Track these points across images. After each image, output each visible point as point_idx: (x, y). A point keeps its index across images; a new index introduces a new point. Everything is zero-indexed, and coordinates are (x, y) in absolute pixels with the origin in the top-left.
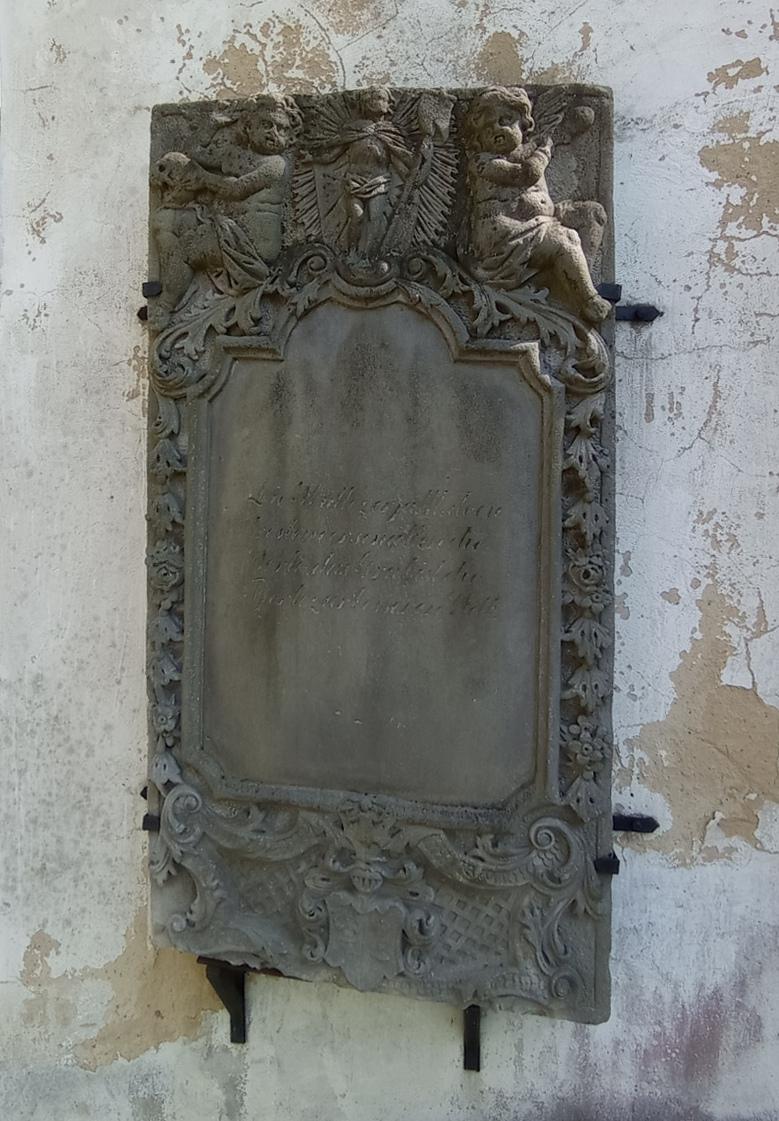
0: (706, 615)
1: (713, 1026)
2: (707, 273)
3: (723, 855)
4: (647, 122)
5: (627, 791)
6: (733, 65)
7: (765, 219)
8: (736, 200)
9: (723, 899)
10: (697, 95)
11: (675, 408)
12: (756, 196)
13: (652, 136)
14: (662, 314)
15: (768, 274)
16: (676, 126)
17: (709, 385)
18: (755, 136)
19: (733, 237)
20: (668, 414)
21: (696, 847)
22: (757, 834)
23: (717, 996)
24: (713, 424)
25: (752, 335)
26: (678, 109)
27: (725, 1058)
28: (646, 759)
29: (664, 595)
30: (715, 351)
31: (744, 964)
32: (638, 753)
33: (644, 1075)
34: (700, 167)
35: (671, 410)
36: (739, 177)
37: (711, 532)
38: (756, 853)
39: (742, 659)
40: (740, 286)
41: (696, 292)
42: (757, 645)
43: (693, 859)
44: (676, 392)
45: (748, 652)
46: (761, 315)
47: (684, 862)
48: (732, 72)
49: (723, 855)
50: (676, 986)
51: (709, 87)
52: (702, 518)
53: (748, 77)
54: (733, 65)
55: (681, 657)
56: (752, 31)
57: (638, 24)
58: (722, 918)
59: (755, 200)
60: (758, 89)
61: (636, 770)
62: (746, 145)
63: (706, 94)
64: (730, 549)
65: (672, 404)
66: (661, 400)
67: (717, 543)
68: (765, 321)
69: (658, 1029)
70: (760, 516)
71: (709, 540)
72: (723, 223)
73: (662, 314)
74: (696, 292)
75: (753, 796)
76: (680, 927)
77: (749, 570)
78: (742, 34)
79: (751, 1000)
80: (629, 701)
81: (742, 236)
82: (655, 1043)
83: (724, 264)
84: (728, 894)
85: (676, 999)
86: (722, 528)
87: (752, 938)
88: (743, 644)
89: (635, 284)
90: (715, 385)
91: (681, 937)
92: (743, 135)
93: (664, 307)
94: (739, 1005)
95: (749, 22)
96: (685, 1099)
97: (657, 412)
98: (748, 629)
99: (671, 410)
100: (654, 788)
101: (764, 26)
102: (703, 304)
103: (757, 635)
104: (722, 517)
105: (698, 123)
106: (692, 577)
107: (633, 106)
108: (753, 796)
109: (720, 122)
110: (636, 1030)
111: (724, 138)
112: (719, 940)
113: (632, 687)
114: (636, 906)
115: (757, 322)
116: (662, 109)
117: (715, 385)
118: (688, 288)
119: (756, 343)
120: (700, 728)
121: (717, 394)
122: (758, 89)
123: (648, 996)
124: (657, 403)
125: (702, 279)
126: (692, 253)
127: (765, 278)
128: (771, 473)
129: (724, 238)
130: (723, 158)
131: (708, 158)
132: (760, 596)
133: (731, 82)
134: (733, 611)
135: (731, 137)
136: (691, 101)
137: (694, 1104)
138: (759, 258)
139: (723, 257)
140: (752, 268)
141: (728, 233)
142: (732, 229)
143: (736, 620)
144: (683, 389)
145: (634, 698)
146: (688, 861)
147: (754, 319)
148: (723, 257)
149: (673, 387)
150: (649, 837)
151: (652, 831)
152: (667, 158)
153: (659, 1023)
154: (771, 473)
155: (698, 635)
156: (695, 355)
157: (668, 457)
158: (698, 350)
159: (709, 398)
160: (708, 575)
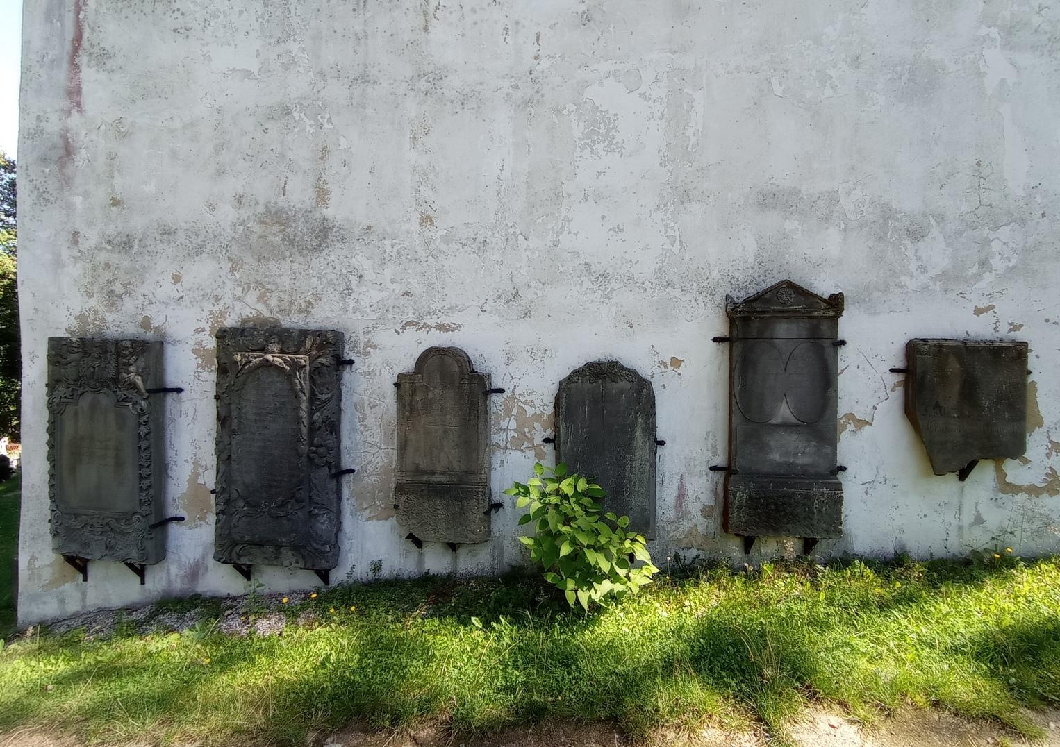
11: (186, 414)
13: (181, 345)
32: (180, 501)
51: (194, 333)
52: (193, 442)
66: (183, 412)
67: (196, 448)
97: (182, 415)
100: (184, 510)
105: (191, 343)
111: (197, 347)
131: (194, 351)
141: (199, 370)
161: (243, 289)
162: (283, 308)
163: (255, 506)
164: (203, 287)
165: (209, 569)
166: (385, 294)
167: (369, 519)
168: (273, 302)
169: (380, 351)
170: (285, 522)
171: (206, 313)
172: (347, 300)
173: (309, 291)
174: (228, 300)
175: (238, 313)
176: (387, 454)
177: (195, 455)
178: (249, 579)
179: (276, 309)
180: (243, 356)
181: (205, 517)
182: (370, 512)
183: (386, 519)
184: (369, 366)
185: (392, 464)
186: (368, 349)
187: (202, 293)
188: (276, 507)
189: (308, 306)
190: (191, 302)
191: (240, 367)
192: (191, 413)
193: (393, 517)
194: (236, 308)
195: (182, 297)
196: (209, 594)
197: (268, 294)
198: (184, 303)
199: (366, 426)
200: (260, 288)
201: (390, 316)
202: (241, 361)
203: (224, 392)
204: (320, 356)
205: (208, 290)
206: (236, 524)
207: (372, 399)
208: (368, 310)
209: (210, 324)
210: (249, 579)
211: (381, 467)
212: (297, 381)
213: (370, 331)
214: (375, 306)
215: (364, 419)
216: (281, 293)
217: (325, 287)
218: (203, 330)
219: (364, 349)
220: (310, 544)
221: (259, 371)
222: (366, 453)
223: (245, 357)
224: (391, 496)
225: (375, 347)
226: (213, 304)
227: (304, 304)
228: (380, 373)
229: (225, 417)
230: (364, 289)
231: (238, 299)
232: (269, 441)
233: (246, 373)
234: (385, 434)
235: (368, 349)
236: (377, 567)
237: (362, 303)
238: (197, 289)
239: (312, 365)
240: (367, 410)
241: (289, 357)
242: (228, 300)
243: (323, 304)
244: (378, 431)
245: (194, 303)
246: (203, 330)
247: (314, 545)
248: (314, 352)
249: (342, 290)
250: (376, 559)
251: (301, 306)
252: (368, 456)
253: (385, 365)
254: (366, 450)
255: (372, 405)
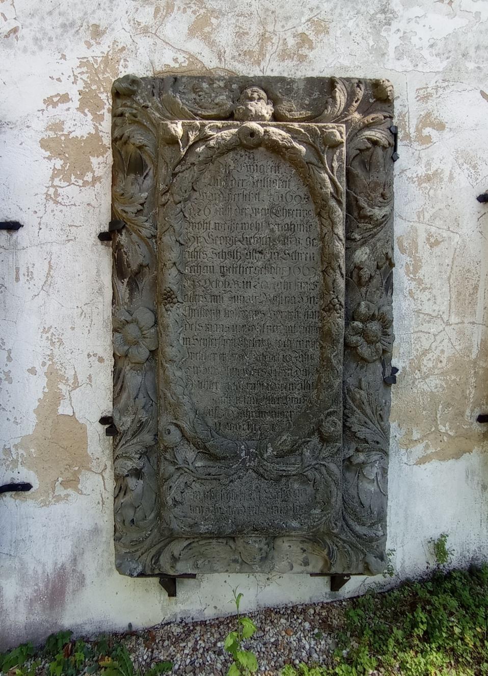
0: (49, 380)
1: (62, 582)
2: (45, 205)
3: (64, 498)
4: (13, 124)
5: (16, 471)
6: (56, 96)
7: (73, 177)
8: (58, 167)
9: (64, 520)
10: (39, 111)
11: (30, 275)
12: (68, 164)
13: (15, 132)
14: (23, 226)
15: (75, 205)
16: (28, 127)
17: (46, 262)
18: (67, 133)
19: (57, 186)
20: (26, 278)
21: (51, 496)
22: (79, 486)
23: (63, 567)
24: (49, 282)
25: (67, 236)
26: (29, 118)
27: (68, 597)
28: (25, 454)
29: (29, 370)
30: (49, 245)
31: (75, 550)
32: (21, 451)
33: (30, 611)
34: (40, 149)
35: (28, 275)
36: (60, 155)
37: (50, 338)
38: (79, 496)
39: (67, 401)
40: (61, 211)
41: (40, 214)
42: (76, 394)
43: (50, 502)
44: (30, 266)
45: (70, 398)
46: (72, 226)
47: (45, 504)
48: (55, 100)
49: (64, 498)
50: (44, 565)
51: (44, 107)
52: (45, 331)
53: (63, 102)
54: (56, 96)
55: (39, 401)
56: (63, 78)
57: (7, 71)
58: (64, 530)
59: (67, 167)
60: (68, 109)
61: (20, 460)
62: (63, 138)
63: (43, 110)
64: (59, 346)
65: (28, 272)
66: (23, 270)
67: (53, 343)
68: (73, 229)
69: (36, 587)
70: (73, 329)
71: (49, 342)
72: (52, 179)
73: (23, 226)
74: (40, 214)
75: (76, 469)
76: (45, 536)
77: (69, 356)
78: (59, 80)
79: (79, 568)
80: (14, 425)
81: (62, 186)
82: (35, 595)
83: (53, 200)
84: (67, 517)
85: (44, 572)
86: (55, 335)
87: (79, 537)
88: (68, 393)
89: (9, 210)
90: (49, 262)
91: (45, 541)
92: (61, 133)
93: (24, 222)
94: (74, 570)
95: (62, 74)
96: (50, 619)
97: (21, 277)
98: (70, 386)
99: (28, 275)
100: (29, 468)
101: (69, 76)
102: (43, 221)
103: (74, 389)
104: (55, 330)
105: (39, 125)
106: (42, 361)
107: (6, 115)
108: (76, 469)
109: (50, 125)
110: (25, 589)
111: (51, 134)
112: (63, 540)
113: (15, 418)
114: (23, 528)
115: (70, 230)
116: (21, 117)
117: (49, 262)
118: (36, 212)
119: (69, 241)
120: (50, 437)
121: (50, 267)
122: (68, 109)
123: (31, 572)
124: (21, 273)
125: (42, 208)
126: (37, 194)
127: (73, 207)
128: (77, 307)
129: (53, 186)
130: (52, 144)
131: (44, 144)
132: (75, 369)
133: (55, 105)
134: (62, 377)
135: (55, 134)
136: (35, 114)
137: (55, 621)
138: (70, 197)
139: (53, 196)
140: (66, 201)
141: (55, 184)
142: (57, 182)
143: (64, 382)
144: (34, 264)
145: (17, 423)
146: (47, 503)
147: (68, 228)
148: (53, 196)
149: (29, 264)
150: (29, 492)
151: (29, 490)
152: (23, 144)
153: (37, 585)
154: (77, 307)
155: (46, 390)
156: (39, 246)
157: (27, 300)
158: (41, 244)
159: (46, 269)
160: (49, 360)
161: (157, 11)
162: (246, 48)
163: (224, 458)
164: (63, 8)
165: (88, 581)
166: (459, 22)
167: (422, 461)
168: (225, 37)
169: (452, 134)
170: (296, 486)
171: (72, 62)
172: (383, 34)
173: (302, 14)
174: (122, 34)
175: (146, 60)
176: (461, 333)
177: (51, 357)
178: (172, 593)
179: (229, 52)
180: (187, 128)
181: (77, 481)
182: (427, 447)
183: (457, 456)
184: (428, 164)
185: (470, 351)
186: (427, 131)
187: (60, 21)
188: (277, 456)
189: (300, 45)
190: (36, 40)
191: (183, 152)
192: (40, 272)
193: (470, 451)
194: (141, 50)
195: (15, 30)
196: (89, 629)
197: (214, 20)
198: (21, 44)
199: (420, 282)
200: (194, 8)
201: (471, 66)
202: (186, 137)
203: (139, 211)
204: (368, 126)
205: (77, 15)
206: (178, 499)
207: (433, 229)
208: (426, 53)
209: (80, 85)
210: (172, 593)
211: (449, 359)
212: (325, 176)
213: (430, 95)
214: (441, 45)
215: (417, 268)
216: (241, 19)
217: (335, 7)
218: (65, 98)
219: (419, 130)
220: (348, 526)
221: (229, 158)
222: (420, 334)
223: (192, 127)
224: (468, 413)
225: (440, 127)
226: (86, 42)
227: (291, 42)
228: (451, 178)
229: (141, 266)
230: (416, 11)
231: (145, 31)
232: (257, 312)
233: (200, 163)
234: (459, 294)
235: (427, 131)
236: (439, 548)
237: (415, 40)
238: (50, 13)
239: (352, 145)
240: (424, 250)
241: (303, 127)
242: (122, 34)
243: (332, 41)
244: (446, 289)
245: (44, 43)
246: (65, 98)
247: (358, 528)
248: (357, 116)
249: (372, 12)
250: (435, 534)
251: (285, 43)
252: (423, 339)
253: (461, 161)
254: (421, 328)
255: (432, 240)
